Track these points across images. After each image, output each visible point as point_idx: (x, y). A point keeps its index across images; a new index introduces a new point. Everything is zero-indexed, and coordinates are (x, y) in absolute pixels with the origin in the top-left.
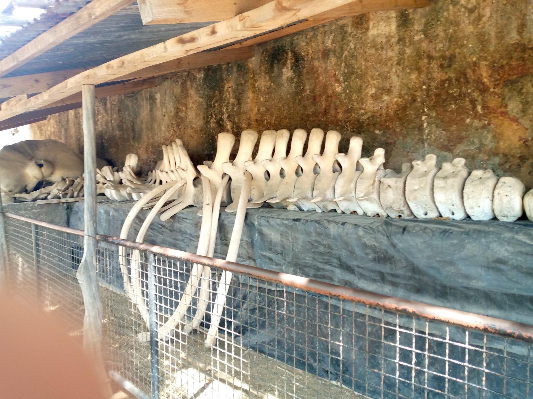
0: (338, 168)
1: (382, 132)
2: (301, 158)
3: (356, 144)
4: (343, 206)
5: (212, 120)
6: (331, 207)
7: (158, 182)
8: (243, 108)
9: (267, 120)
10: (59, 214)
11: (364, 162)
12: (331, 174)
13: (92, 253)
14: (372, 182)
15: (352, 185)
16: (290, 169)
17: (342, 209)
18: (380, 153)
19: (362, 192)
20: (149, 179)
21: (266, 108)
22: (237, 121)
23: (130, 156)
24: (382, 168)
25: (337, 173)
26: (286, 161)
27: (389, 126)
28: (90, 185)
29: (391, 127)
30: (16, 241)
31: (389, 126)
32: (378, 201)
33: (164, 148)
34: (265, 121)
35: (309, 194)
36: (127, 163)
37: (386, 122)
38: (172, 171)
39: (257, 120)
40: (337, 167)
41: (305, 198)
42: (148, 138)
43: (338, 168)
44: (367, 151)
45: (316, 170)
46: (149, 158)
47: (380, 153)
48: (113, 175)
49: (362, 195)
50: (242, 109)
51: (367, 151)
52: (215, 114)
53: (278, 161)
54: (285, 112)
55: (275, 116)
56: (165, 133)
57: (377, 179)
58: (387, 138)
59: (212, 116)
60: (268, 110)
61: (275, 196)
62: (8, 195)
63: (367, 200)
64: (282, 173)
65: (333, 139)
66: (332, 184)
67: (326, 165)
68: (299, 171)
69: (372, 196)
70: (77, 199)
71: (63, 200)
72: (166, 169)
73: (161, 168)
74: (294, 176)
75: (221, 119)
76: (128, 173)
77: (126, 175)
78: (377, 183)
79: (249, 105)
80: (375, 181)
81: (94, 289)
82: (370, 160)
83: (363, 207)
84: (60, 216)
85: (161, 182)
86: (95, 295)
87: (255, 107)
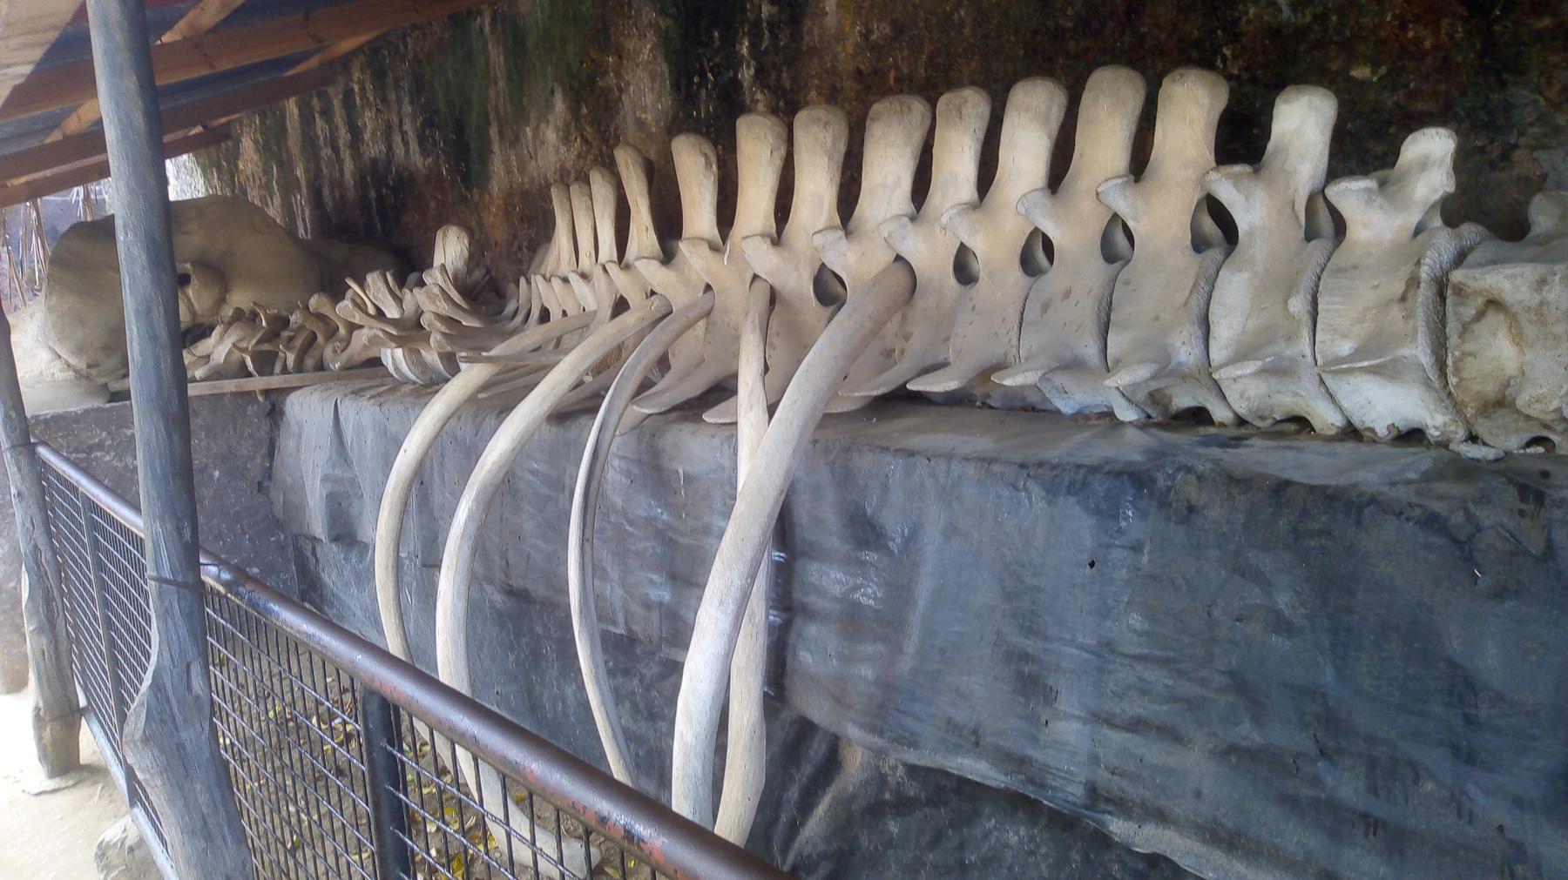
0: (1217, 228)
1: (1383, 70)
2: (1043, 199)
3: (1303, 122)
4: (1244, 391)
5: (703, 93)
6: (1183, 400)
7: (535, 313)
8: (810, 32)
9: (898, 69)
10: (248, 430)
11: (1351, 195)
12: (1184, 262)
13: (182, 651)
14: (1399, 287)
15: (1298, 305)
16: (994, 246)
17: (1242, 408)
18: (1431, 154)
19: (1345, 336)
20: (510, 308)
21: (894, 23)
22: (788, 85)
23: (445, 235)
24: (1437, 222)
25: (1215, 254)
26: (976, 215)
27: (1418, 41)
28: (151, 362)
29: (1427, 44)
30: (67, 539)
31: (1418, 41)
32: (1433, 375)
33: (555, 193)
34: (892, 74)
35: (1090, 350)
36: (438, 259)
37: (1403, 26)
38: (584, 276)
39: (859, 72)
40: (1209, 226)
41: (1074, 365)
42: (509, 171)
43: (1217, 228)
44: (1363, 147)
45: (1116, 242)
46: (515, 237)
47: (1431, 154)
48: (399, 301)
49: (1345, 348)
50: (807, 38)
51: (1363, 147)
52: (711, 71)
53: (944, 219)
54: (967, 31)
55: (927, 48)
56: (557, 151)
57: (1425, 272)
58: (1411, 95)
59: (703, 76)
60: (898, 29)
61: (941, 358)
62: (87, 378)
63: (1374, 371)
64: (963, 268)
65: (1192, 108)
66: (1196, 302)
67: (1161, 217)
68: (1036, 253)
69: (1405, 351)
70: (293, 379)
71: (258, 383)
72: (566, 268)
73: (549, 265)
74: (1016, 275)
75: (736, 84)
76: (436, 290)
77: (432, 297)
78: (1425, 293)
79: (831, 21)
80: (1413, 282)
81: (203, 799)
82: (1382, 184)
83: (1345, 404)
84: (251, 436)
85: (545, 316)
86: (211, 822)
87: (853, 25)
